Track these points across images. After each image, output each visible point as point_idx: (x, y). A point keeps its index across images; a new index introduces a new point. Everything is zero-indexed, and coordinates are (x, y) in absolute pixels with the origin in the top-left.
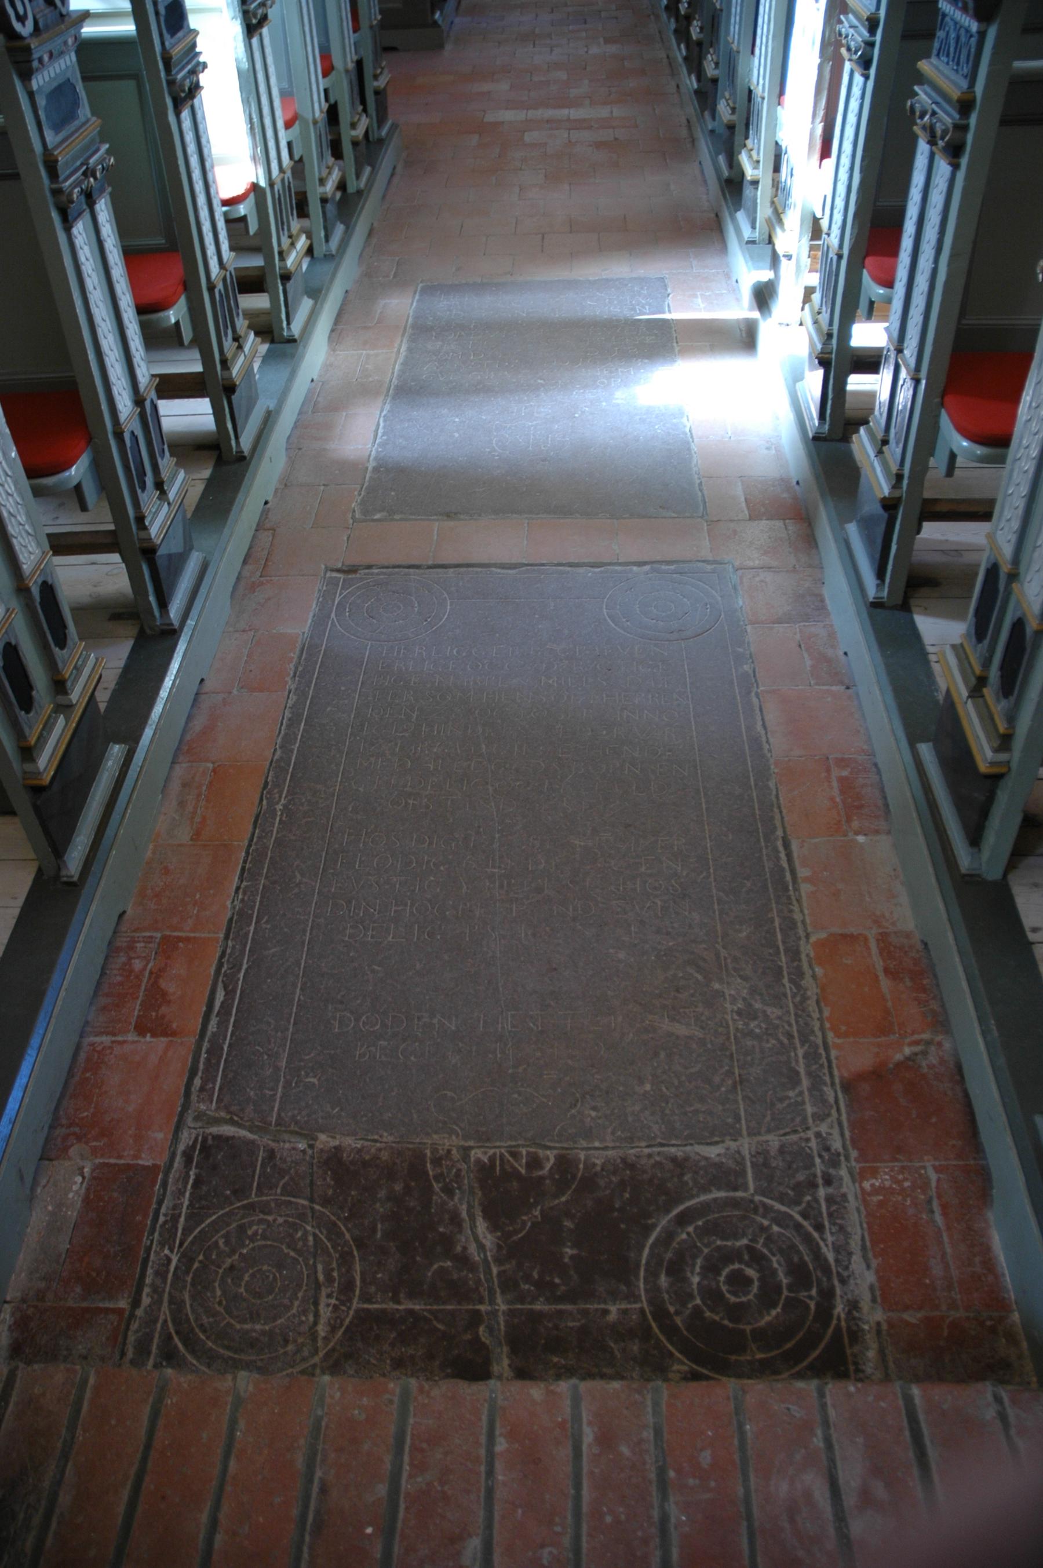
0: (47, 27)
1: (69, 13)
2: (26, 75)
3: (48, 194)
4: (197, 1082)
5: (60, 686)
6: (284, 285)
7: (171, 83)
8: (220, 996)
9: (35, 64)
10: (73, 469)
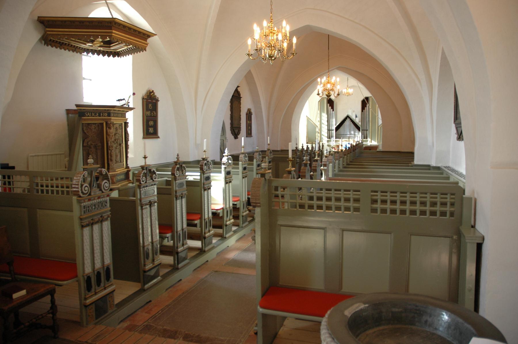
0: (181, 176)
1: (185, 175)
2: (176, 181)
3: (174, 195)
4: (151, 319)
5: (153, 260)
6: (226, 227)
7: (204, 187)
8: (160, 312)
9: (177, 180)
10: (168, 235)
